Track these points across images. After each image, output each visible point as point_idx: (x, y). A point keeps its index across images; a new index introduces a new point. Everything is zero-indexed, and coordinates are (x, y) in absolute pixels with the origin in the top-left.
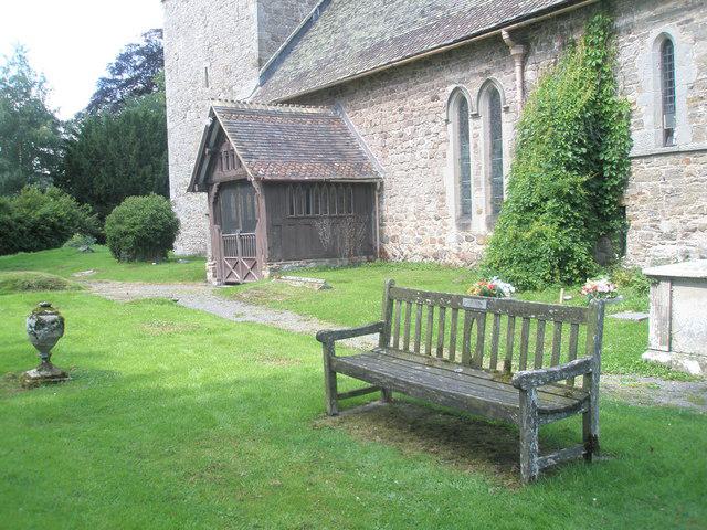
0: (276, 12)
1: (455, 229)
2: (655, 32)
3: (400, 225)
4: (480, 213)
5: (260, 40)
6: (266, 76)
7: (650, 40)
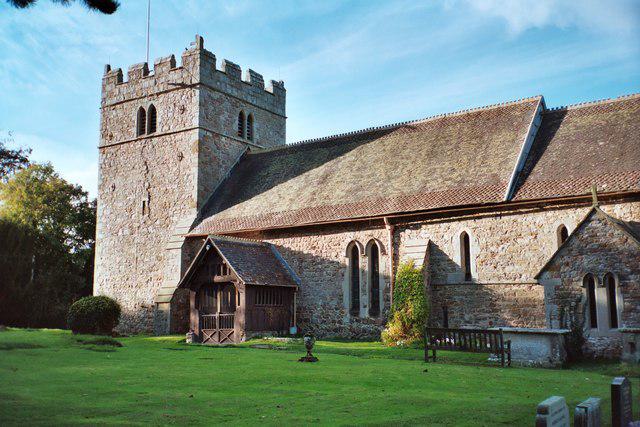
1: (348, 315)
4: (365, 307)
5: (199, 191)
6: (205, 209)
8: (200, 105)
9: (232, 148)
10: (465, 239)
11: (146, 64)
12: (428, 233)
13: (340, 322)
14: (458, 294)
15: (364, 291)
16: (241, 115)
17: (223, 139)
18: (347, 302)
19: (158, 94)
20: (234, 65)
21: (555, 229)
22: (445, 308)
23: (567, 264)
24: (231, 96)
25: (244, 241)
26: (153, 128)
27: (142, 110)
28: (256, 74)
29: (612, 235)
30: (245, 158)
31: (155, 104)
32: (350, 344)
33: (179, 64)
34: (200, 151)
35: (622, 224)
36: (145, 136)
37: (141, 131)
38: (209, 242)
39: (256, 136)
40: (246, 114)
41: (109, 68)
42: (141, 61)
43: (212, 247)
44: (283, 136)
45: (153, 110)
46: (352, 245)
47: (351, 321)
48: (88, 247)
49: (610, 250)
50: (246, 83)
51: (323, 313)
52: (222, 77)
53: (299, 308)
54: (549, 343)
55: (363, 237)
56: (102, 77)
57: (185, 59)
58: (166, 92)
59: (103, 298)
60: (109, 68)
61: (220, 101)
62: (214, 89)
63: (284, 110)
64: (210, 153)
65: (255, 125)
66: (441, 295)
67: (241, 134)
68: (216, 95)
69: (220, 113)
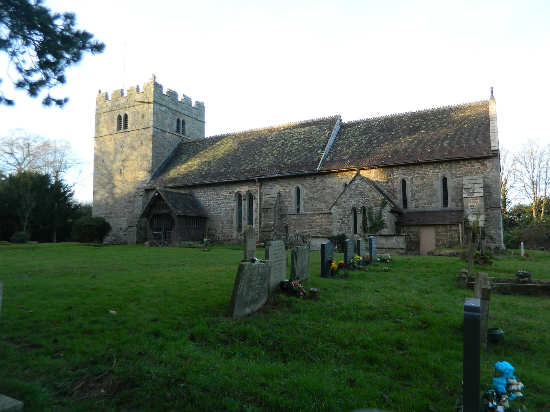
0: (158, 153)
1: (236, 232)
2: (296, 186)
3: (216, 231)
7: (294, 187)
8: (153, 114)
9: (172, 139)
10: (298, 190)
11: (122, 90)
12: (277, 188)
13: (231, 236)
14: (293, 220)
15: (244, 219)
16: (178, 120)
17: (167, 134)
18: (235, 224)
19: (129, 107)
20: (174, 92)
21: (117, 116)
22: (286, 227)
23: (344, 202)
24: (172, 109)
25: (178, 191)
26: (126, 127)
27: (119, 117)
28: (188, 97)
29: (365, 187)
30: (180, 145)
31: (127, 113)
32: (170, 191)
33: (141, 90)
34: (153, 140)
35: (370, 182)
36: (122, 130)
37: (119, 128)
38: (157, 192)
39: (187, 132)
40: (181, 120)
41: (100, 92)
42: (119, 88)
43: (159, 195)
44: (203, 133)
45: (126, 116)
46: (238, 194)
47: (237, 235)
48: (12, 10)
49: (364, 195)
50: (179, 101)
51: (222, 231)
52: (167, 98)
53: (209, 229)
54: (41, 88)
55: (244, 189)
56: (97, 97)
57: (145, 89)
58: (134, 106)
59: (98, 218)
60: (100, 92)
61: (165, 112)
62: (161, 105)
63: (204, 118)
64: (159, 142)
65: (187, 126)
66: (284, 220)
67: (178, 131)
68: (163, 109)
69: (166, 118)
